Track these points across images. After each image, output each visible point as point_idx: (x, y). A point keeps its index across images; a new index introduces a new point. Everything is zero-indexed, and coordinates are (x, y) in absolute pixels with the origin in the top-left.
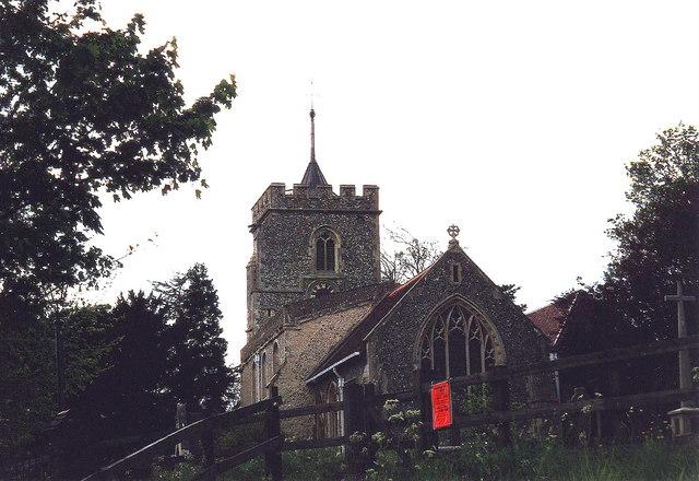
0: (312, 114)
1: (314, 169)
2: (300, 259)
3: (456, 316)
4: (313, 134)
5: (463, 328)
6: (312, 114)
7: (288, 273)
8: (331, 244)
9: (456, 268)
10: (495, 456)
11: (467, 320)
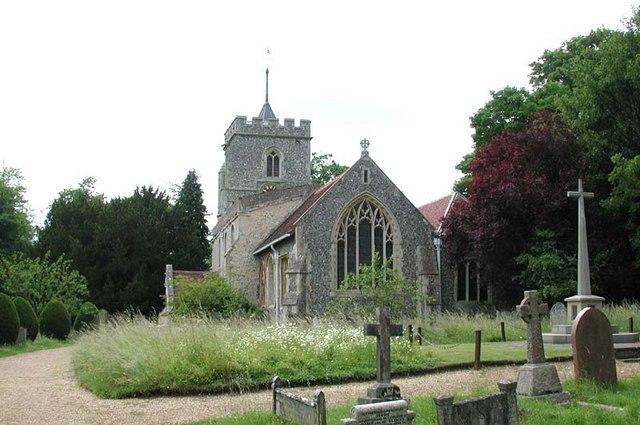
0: (267, 72)
3: (365, 208)
6: (267, 72)
8: (277, 159)
9: (366, 172)
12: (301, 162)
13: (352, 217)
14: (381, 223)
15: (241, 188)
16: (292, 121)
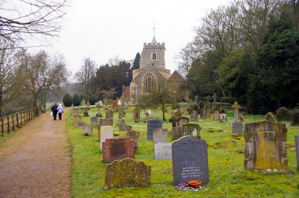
0: (154, 28)
2: (9, 158)
3: (150, 75)
6: (154, 28)
7: (147, 60)
8: (155, 54)
10: (254, 107)
13: (146, 77)
15: (145, 63)
16: (160, 43)
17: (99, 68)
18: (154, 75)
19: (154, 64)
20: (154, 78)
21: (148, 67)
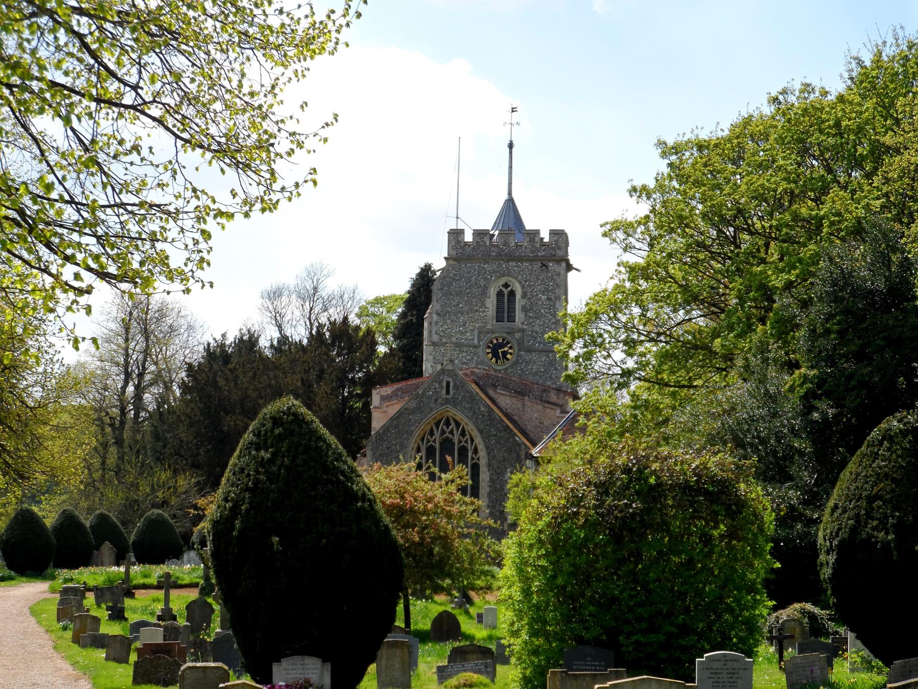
0: (511, 146)
1: (510, 207)
2: (477, 311)
3: (448, 423)
4: (511, 167)
5: (453, 435)
6: (511, 146)
7: (464, 325)
8: (512, 294)
9: (448, 383)
11: (458, 429)
12: (549, 299)
13: (432, 433)
14: (466, 442)
17: (197, 356)
18: (470, 427)
19: (501, 346)
20: (472, 441)
21: (440, 382)
